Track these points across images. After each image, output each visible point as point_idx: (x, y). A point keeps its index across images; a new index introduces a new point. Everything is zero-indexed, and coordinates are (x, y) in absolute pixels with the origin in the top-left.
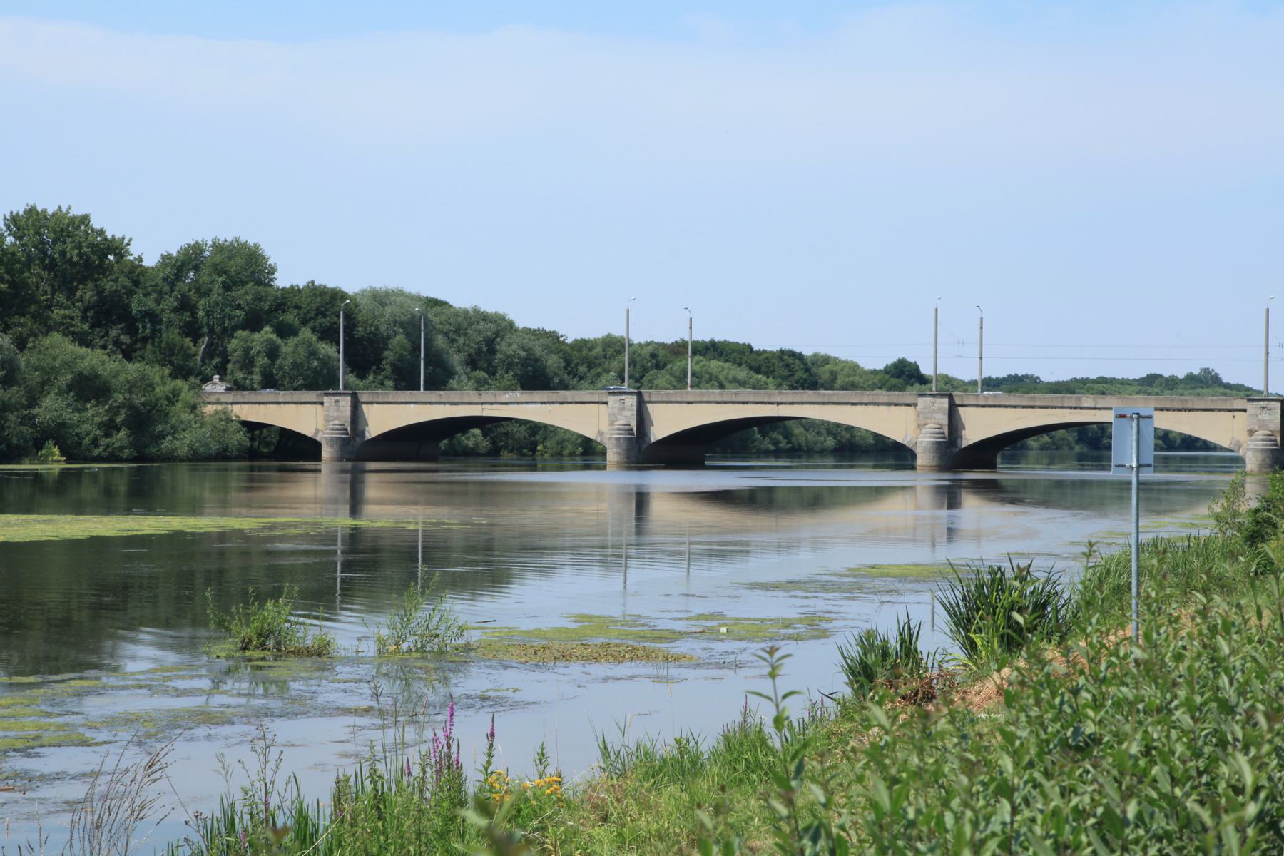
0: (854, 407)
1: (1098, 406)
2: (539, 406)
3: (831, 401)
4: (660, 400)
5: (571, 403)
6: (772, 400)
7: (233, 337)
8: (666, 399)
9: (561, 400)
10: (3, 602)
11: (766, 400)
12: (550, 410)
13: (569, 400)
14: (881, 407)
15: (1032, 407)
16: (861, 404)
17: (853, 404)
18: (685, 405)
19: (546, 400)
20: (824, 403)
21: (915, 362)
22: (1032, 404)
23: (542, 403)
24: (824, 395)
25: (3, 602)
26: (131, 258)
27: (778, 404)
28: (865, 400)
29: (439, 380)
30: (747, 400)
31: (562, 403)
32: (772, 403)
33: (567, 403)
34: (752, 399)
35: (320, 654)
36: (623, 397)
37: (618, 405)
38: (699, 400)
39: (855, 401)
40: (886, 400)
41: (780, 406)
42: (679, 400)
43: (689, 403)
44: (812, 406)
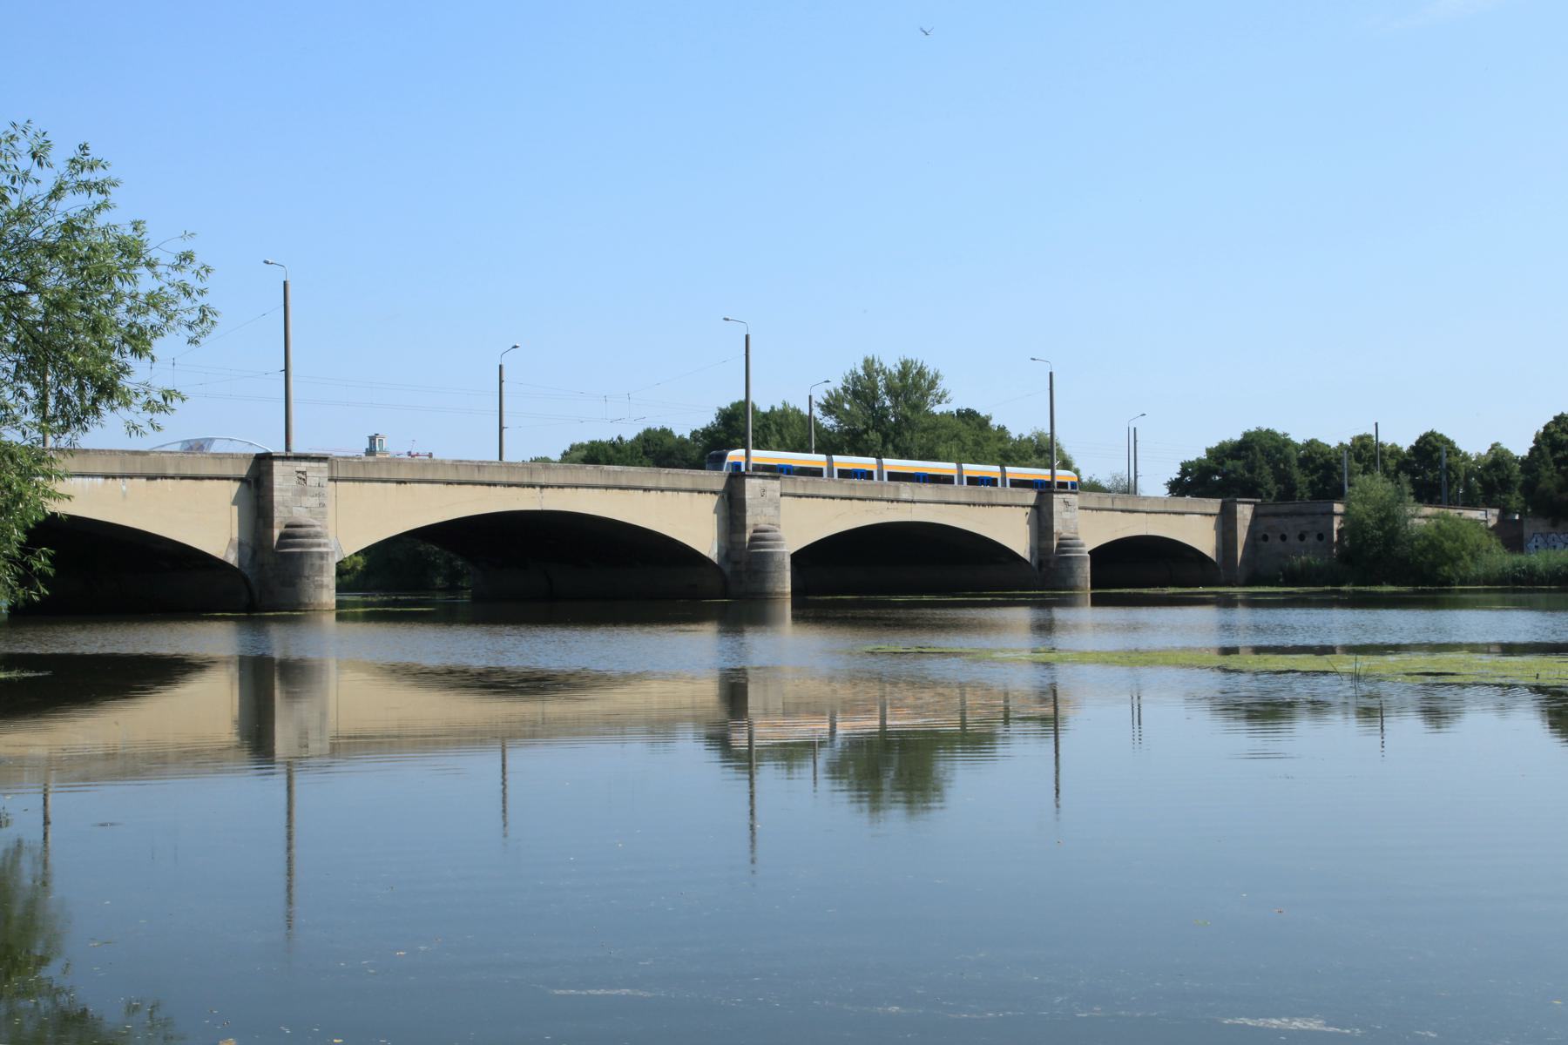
0: (647, 493)
1: (915, 498)
2: (100, 480)
3: (618, 483)
4: (350, 475)
5: (173, 478)
6: (535, 480)
7: (882, 790)
8: (361, 475)
9: (152, 471)
10: (1566, 631)
11: (526, 480)
12: (125, 495)
13: (171, 472)
14: (682, 494)
15: (851, 499)
16: (656, 489)
17: (645, 490)
18: (442, 486)
19: (117, 470)
20: (607, 488)
21: (1494, 446)
22: (852, 494)
23: (106, 477)
24: (608, 473)
25: (1566, 631)
26: (937, 409)
27: (542, 487)
28: (663, 484)
29: (802, 448)
30: (496, 479)
31: (151, 478)
32: (533, 486)
33: (166, 478)
34: (504, 479)
35: (1076, 627)
36: (303, 465)
37: (294, 481)
38: (418, 477)
39: (649, 484)
40: (687, 484)
41: (546, 491)
42: (384, 476)
43: (399, 482)
44: (590, 490)
